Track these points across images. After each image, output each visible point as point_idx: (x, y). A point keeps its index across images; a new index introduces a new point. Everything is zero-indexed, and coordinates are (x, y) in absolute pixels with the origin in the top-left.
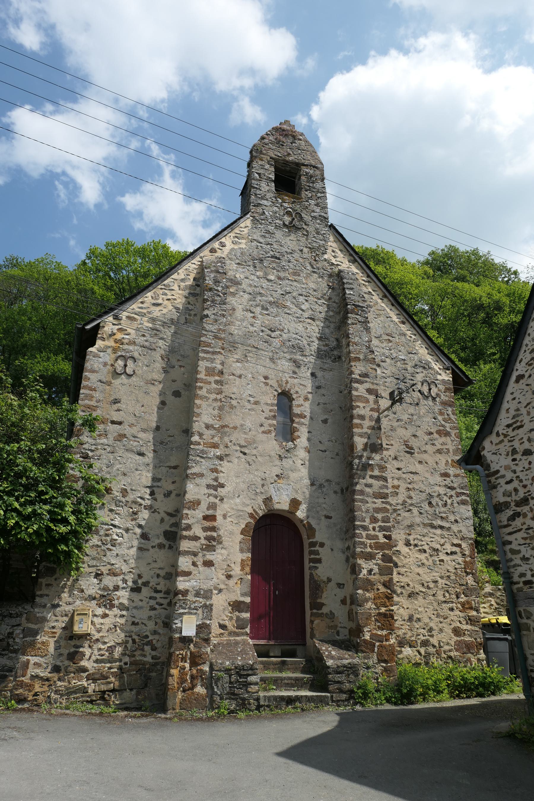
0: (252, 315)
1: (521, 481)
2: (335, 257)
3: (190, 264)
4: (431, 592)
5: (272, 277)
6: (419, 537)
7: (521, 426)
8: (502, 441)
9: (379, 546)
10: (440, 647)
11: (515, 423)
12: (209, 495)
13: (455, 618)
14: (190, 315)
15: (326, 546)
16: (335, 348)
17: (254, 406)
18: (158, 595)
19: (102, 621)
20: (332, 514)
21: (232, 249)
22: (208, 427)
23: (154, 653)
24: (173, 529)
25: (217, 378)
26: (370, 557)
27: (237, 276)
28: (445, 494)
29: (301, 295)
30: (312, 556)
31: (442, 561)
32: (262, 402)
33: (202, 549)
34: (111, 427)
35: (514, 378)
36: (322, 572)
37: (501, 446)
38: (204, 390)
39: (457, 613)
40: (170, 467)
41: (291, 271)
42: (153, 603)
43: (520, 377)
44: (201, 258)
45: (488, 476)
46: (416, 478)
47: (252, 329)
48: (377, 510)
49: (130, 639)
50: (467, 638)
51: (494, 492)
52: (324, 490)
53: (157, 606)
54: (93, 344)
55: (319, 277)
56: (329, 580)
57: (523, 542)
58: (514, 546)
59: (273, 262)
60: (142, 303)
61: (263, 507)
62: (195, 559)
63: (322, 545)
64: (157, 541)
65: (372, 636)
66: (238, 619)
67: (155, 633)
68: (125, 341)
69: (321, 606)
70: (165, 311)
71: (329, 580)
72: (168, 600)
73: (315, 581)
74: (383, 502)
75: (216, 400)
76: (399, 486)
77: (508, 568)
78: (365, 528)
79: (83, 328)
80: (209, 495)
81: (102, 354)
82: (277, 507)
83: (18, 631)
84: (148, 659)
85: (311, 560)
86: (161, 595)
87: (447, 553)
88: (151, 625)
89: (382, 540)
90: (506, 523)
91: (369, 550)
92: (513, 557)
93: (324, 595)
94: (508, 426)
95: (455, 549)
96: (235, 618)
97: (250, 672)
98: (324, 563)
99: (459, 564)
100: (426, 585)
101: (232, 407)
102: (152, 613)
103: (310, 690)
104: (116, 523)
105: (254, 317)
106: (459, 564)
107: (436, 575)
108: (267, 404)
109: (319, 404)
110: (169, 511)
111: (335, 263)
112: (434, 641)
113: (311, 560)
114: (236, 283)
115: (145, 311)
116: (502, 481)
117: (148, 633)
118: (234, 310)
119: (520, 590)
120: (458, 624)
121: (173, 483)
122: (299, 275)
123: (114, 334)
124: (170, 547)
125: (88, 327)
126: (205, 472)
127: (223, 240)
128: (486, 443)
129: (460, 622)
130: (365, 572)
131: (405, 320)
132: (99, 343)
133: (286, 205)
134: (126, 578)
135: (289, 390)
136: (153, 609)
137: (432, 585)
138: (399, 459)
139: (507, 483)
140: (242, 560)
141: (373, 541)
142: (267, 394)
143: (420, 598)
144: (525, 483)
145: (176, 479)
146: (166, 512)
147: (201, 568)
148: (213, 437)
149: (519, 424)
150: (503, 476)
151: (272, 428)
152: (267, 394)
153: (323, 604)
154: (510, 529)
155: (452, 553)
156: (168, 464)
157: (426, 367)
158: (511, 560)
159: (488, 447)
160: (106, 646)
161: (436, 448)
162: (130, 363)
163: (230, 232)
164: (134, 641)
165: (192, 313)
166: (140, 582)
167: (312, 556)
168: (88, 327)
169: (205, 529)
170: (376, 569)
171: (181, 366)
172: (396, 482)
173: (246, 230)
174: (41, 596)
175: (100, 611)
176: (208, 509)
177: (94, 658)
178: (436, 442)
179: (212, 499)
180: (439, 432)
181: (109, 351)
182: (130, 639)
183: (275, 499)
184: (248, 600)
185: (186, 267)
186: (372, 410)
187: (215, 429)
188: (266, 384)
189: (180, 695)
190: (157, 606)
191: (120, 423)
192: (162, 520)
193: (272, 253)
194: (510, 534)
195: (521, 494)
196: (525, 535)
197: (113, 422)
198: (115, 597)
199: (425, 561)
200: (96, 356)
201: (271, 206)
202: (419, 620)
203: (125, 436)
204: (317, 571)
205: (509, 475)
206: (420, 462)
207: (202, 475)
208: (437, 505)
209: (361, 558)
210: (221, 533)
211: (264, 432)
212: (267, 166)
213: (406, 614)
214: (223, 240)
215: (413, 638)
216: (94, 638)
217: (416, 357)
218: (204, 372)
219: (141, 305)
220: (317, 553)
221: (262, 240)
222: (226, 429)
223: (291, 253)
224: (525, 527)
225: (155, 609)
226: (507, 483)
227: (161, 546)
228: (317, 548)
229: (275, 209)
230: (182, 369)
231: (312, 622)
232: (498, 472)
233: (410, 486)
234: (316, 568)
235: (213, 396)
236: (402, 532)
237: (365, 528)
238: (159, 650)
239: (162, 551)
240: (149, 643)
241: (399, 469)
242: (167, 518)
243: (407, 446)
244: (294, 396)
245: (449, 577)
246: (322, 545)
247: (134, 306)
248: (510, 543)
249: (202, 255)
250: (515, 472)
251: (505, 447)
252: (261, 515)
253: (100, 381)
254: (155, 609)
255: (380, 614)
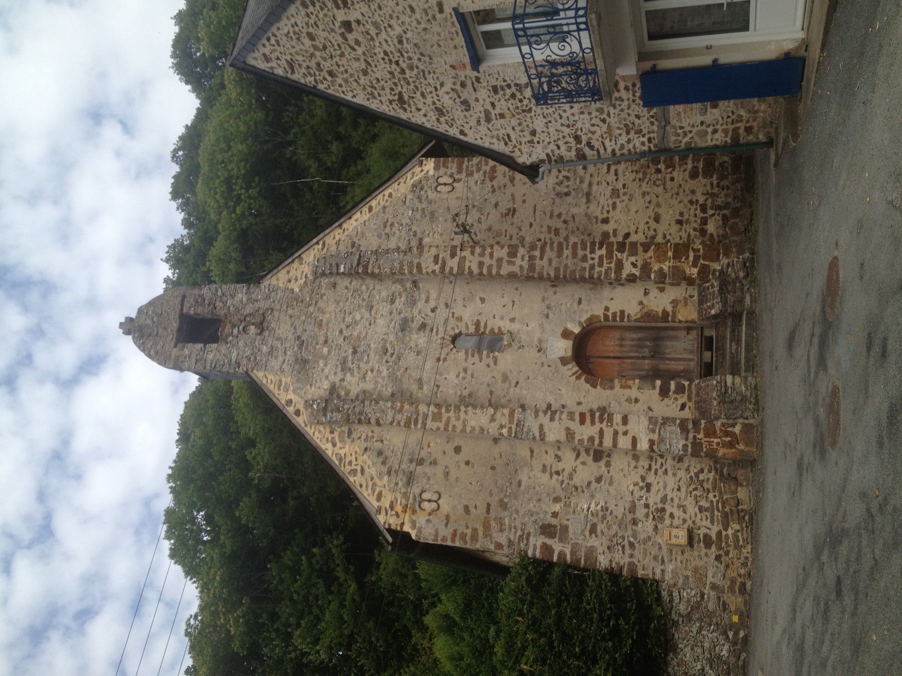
0: (369, 373)
1: (559, 139)
2: (296, 280)
3: (315, 438)
4: (655, 200)
5: (325, 350)
6: (600, 208)
7: (508, 136)
8: (520, 150)
9: (610, 255)
10: (708, 193)
11: (504, 139)
12: (560, 419)
13: (681, 176)
14: (373, 437)
15: (609, 306)
16: (403, 286)
17: (469, 373)
18: (654, 467)
19: (676, 518)
20: (577, 297)
21: (294, 391)
22: (493, 420)
23: (706, 471)
24: (592, 453)
25: (443, 410)
26: (620, 265)
27: (326, 387)
28: (557, 177)
29: (344, 318)
30: (618, 319)
31: (624, 186)
32: (464, 364)
33: (612, 426)
34: (493, 514)
35: (462, 137)
36: (633, 310)
37: (524, 150)
38: (456, 423)
39: (675, 174)
40: (532, 456)
41: (316, 330)
42: (660, 472)
43: (462, 132)
44: (306, 425)
45: (550, 161)
46: (539, 208)
47: (385, 373)
48: (575, 255)
49: (693, 493)
50: (701, 165)
51: (565, 159)
52: (553, 304)
53: (664, 468)
54: (408, 535)
55: (322, 298)
56: (641, 303)
57: (613, 142)
58: (617, 148)
59: (307, 348)
60: (361, 486)
61: (570, 366)
62: (621, 432)
63: (607, 309)
64: (603, 468)
65: (695, 265)
66: (676, 392)
67: (688, 470)
68: (404, 502)
69: (665, 314)
70: (369, 462)
71: (641, 303)
72: (658, 458)
73: (642, 317)
74: (567, 249)
75: (466, 412)
76: (548, 227)
77: (636, 153)
78: (592, 267)
79: (391, 544)
80: (560, 419)
81: (418, 525)
82: (570, 353)
83: (685, 594)
84: (711, 476)
85: (622, 320)
86: (653, 464)
87: (616, 180)
88: (681, 474)
89: (603, 251)
90: (595, 152)
91: (613, 265)
92: (626, 149)
93: (655, 308)
94: (506, 144)
95: (612, 171)
96: (675, 396)
97: (723, 385)
98: (625, 308)
99: (627, 168)
100: (647, 204)
101: (470, 395)
102: (670, 473)
103: (741, 326)
104: (585, 507)
105: (372, 371)
106: (627, 168)
107: (638, 194)
108: (466, 359)
109: (465, 306)
110: (574, 456)
111: (304, 279)
112: (701, 200)
113: (622, 320)
114: (333, 389)
115: (370, 484)
116: (557, 152)
117: (688, 476)
118: (365, 391)
119: (655, 146)
120: (687, 173)
121: (547, 453)
122: (321, 320)
123: (397, 513)
124: (609, 456)
125: (390, 539)
126: (539, 423)
127: (283, 402)
128: (520, 160)
129: (685, 171)
130: (634, 271)
131: (367, 206)
132: (407, 528)
133: (235, 331)
134: (637, 497)
135: (450, 336)
136: (666, 472)
137: (648, 198)
138: (520, 224)
139: (559, 148)
140: (621, 387)
141: (605, 261)
142: (455, 359)
143: (660, 211)
144: (561, 136)
145: (543, 450)
146: (576, 460)
147: (628, 427)
148: (503, 414)
149: (506, 137)
150: (553, 151)
151: (491, 355)
152: (455, 359)
153: (664, 310)
154: (602, 151)
155: (616, 174)
156: (529, 458)
157: (417, 187)
158: (629, 150)
159: (523, 159)
160: (699, 515)
161: (509, 183)
162: (425, 496)
163: (274, 395)
164: (696, 489)
165: (370, 434)
166: (641, 484)
167: (618, 319)
168: (390, 539)
169: (593, 423)
170: (633, 259)
171: (429, 446)
172: (545, 229)
173: (270, 377)
174: (654, 574)
175: (668, 521)
176: (574, 420)
177: (709, 525)
178: (502, 183)
179: (564, 416)
180: (492, 179)
181: (414, 518)
182: (693, 493)
183: (562, 354)
184: (658, 383)
185: (318, 441)
186: (473, 253)
187: (495, 413)
188: (445, 360)
189: (741, 447)
190: (664, 468)
191: (489, 505)
192: (583, 463)
193: (296, 348)
194: (605, 149)
195: (572, 140)
196: (608, 139)
197: (488, 512)
198: (655, 507)
199: (624, 204)
200: (420, 530)
201: (238, 349)
202: (681, 214)
203: (501, 501)
204: (632, 315)
205: (553, 146)
206: (524, 202)
207: (541, 427)
208: (568, 187)
209: (621, 274)
210: (595, 407)
211: (495, 364)
212: (186, 352)
213: (675, 228)
214: (283, 402)
215: (699, 221)
216: (692, 525)
217: (409, 197)
218: (438, 424)
219: (364, 487)
220: (614, 314)
221: (281, 359)
222: (493, 401)
223: (295, 328)
224: (600, 139)
225: (666, 470)
226: (559, 148)
227: (608, 464)
228: (610, 314)
229: (241, 344)
230: (432, 444)
231: (680, 322)
232: (547, 155)
233: (548, 215)
234: (629, 316)
235: (462, 414)
236: (595, 226)
237: (592, 267)
238: (703, 466)
239: (612, 463)
240: (697, 475)
241: (531, 225)
242: (581, 459)
243: (507, 214)
244: (457, 331)
245: (640, 180)
246: (607, 309)
247: (365, 494)
248: (613, 150)
249: (303, 425)
250: (549, 143)
251: (525, 148)
252: (577, 368)
253: (446, 525)
254: (666, 470)
255: (674, 258)
